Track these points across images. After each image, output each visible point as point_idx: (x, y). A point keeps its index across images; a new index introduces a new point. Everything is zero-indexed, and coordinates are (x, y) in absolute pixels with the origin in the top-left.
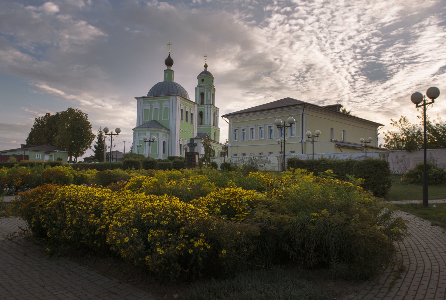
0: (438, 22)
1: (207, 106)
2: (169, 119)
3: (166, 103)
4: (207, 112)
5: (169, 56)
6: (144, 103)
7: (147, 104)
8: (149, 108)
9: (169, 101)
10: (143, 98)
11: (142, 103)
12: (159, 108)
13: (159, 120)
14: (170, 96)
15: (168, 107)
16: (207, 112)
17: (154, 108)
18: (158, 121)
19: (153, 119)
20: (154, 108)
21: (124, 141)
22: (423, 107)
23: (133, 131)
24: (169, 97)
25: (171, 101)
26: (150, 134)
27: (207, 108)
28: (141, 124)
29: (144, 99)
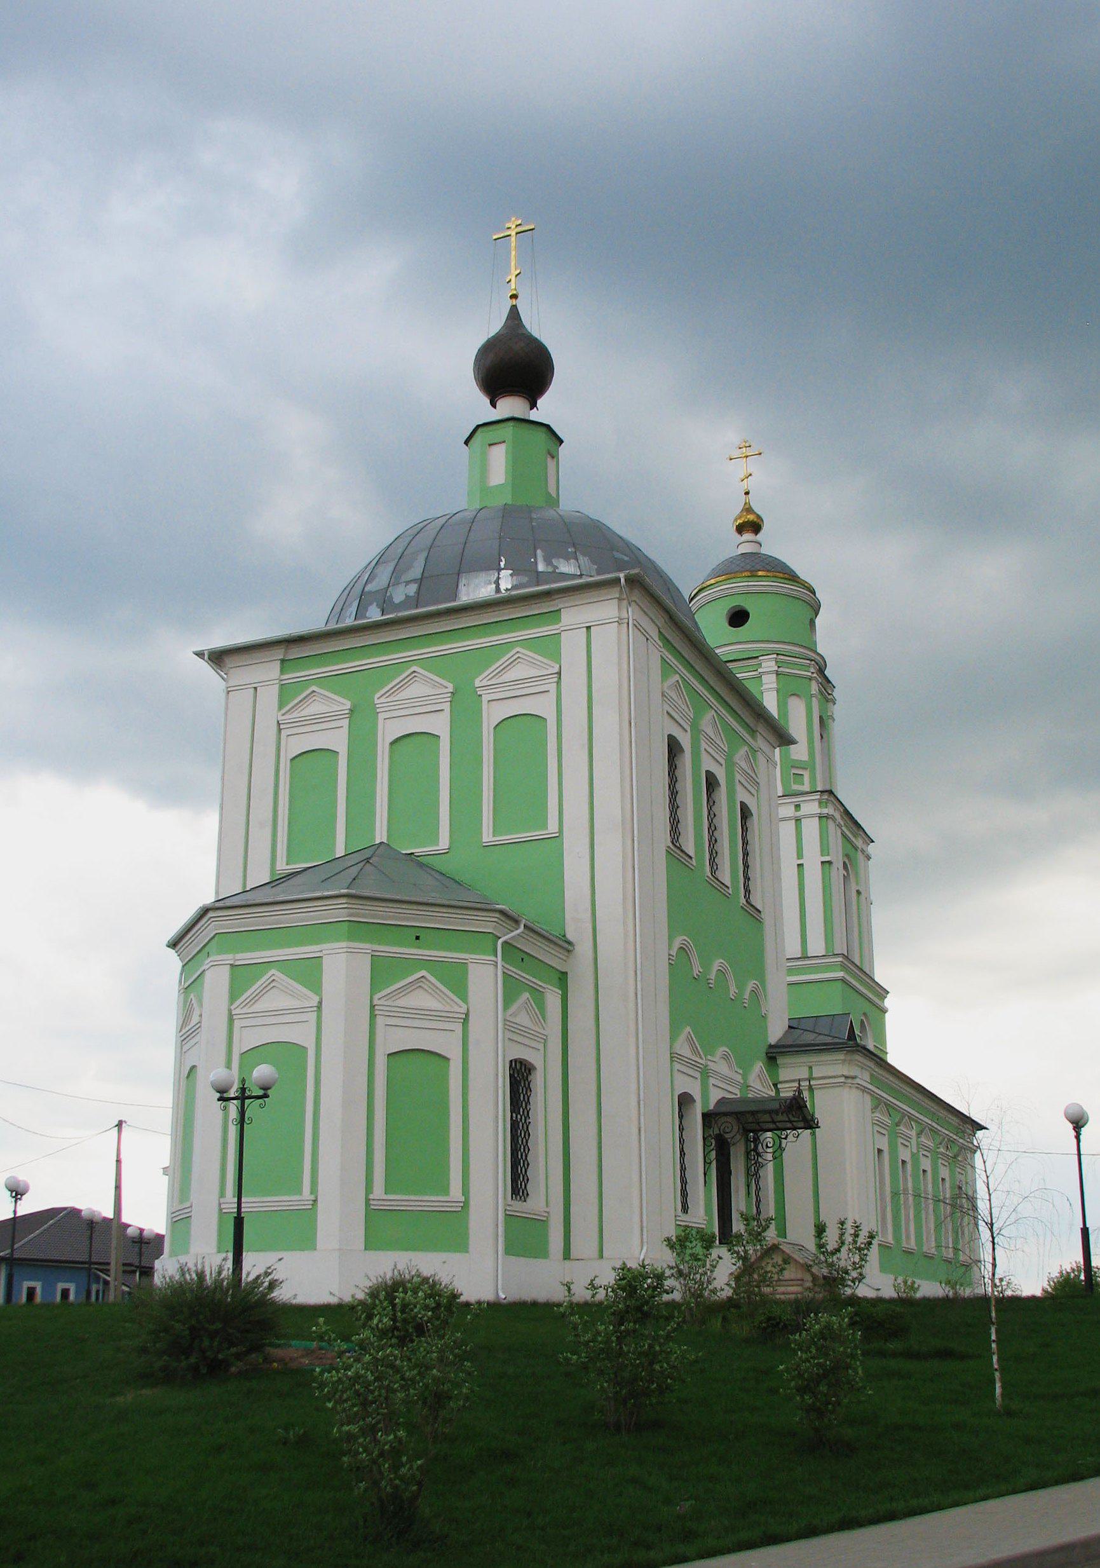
0: (208, 1273)
1: (798, 807)
2: (553, 827)
3: (519, 672)
4: (800, 855)
5: (514, 313)
6: (285, 694)
7: (316, 708)
8: (337, 739)
9: (550, 647)
10: (279, 653)
11: (269, 695)
12: (440, 725)
13: (444, 843)
14: (558, 604)
15: (543, 706)
16: (800, 855)
17: (389, 729)
18: (436, 862)
19: (380, 836)
20: (389, 729)
21: (120, 1125)
22: (787, 1119)
23: (173, 961)
24: (546, 607)
25: (572, 645)
26: (364, 964)
27: (798, 820)
28: (260, 875)
29: (296, 652)
